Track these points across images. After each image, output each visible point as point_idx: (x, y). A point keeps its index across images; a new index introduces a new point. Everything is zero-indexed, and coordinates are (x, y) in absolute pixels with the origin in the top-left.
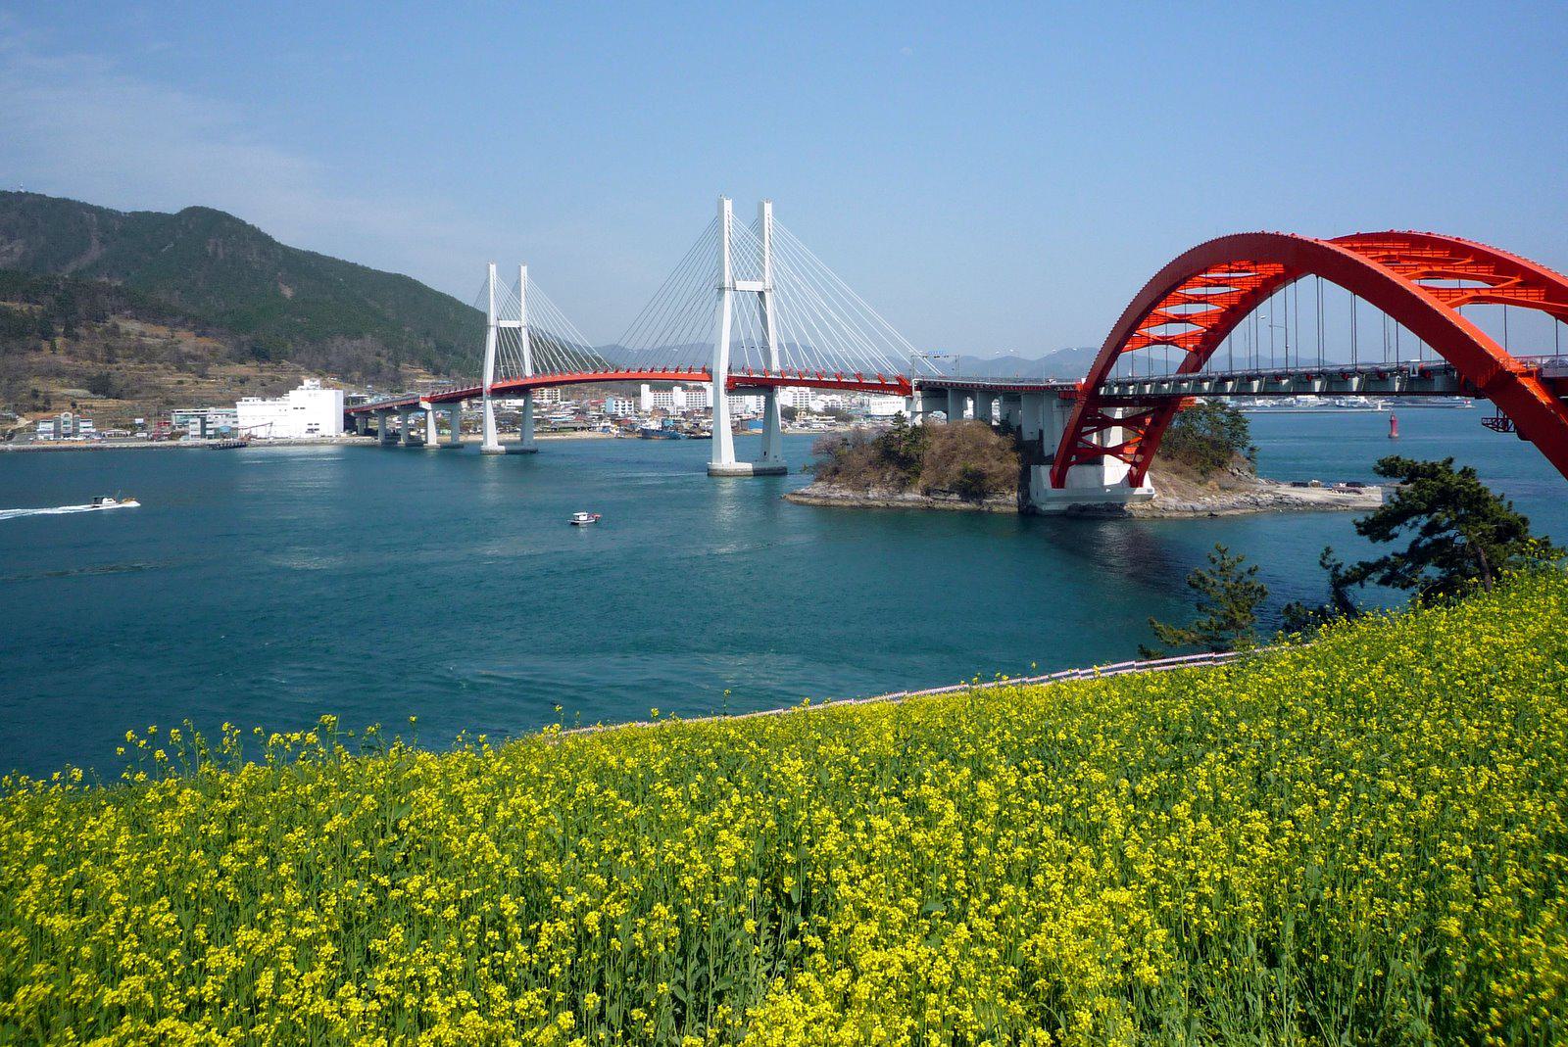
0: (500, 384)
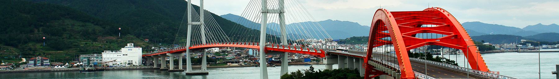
0: (193, 47)
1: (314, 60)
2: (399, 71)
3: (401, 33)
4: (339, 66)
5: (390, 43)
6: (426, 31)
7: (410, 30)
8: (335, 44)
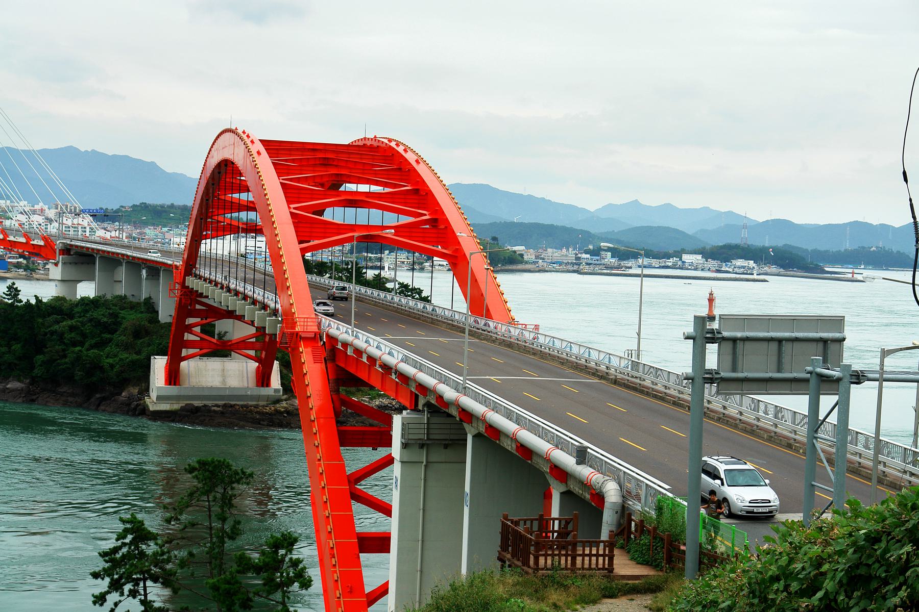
1: (18, 266)
2: (275, 312)
3: (289, 202)
4: (98, 289)
5: (253, 229)
6: (355, 201)
7: (313, 195)
8: (86, 221)
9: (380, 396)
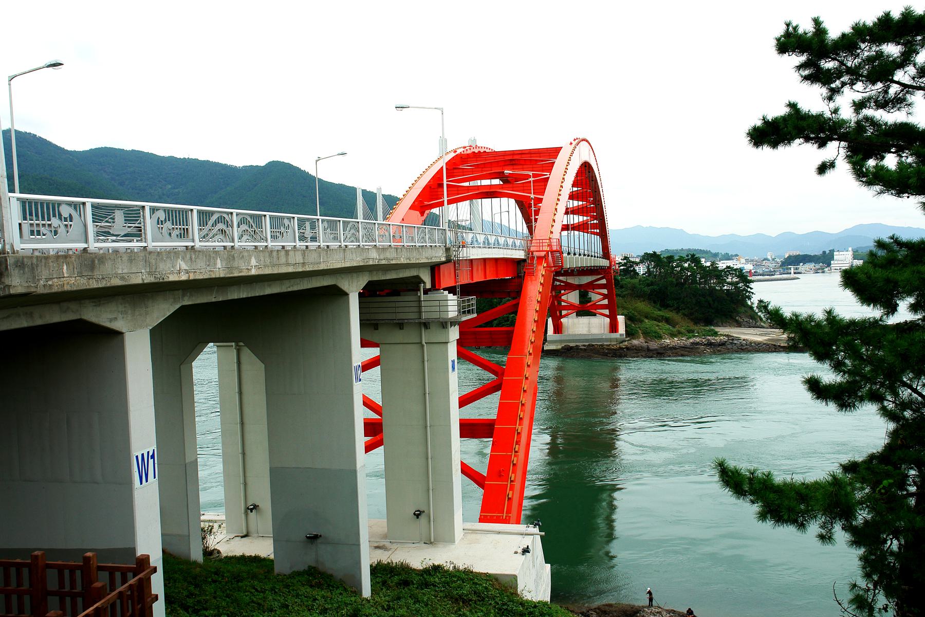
9: (695, 336)
